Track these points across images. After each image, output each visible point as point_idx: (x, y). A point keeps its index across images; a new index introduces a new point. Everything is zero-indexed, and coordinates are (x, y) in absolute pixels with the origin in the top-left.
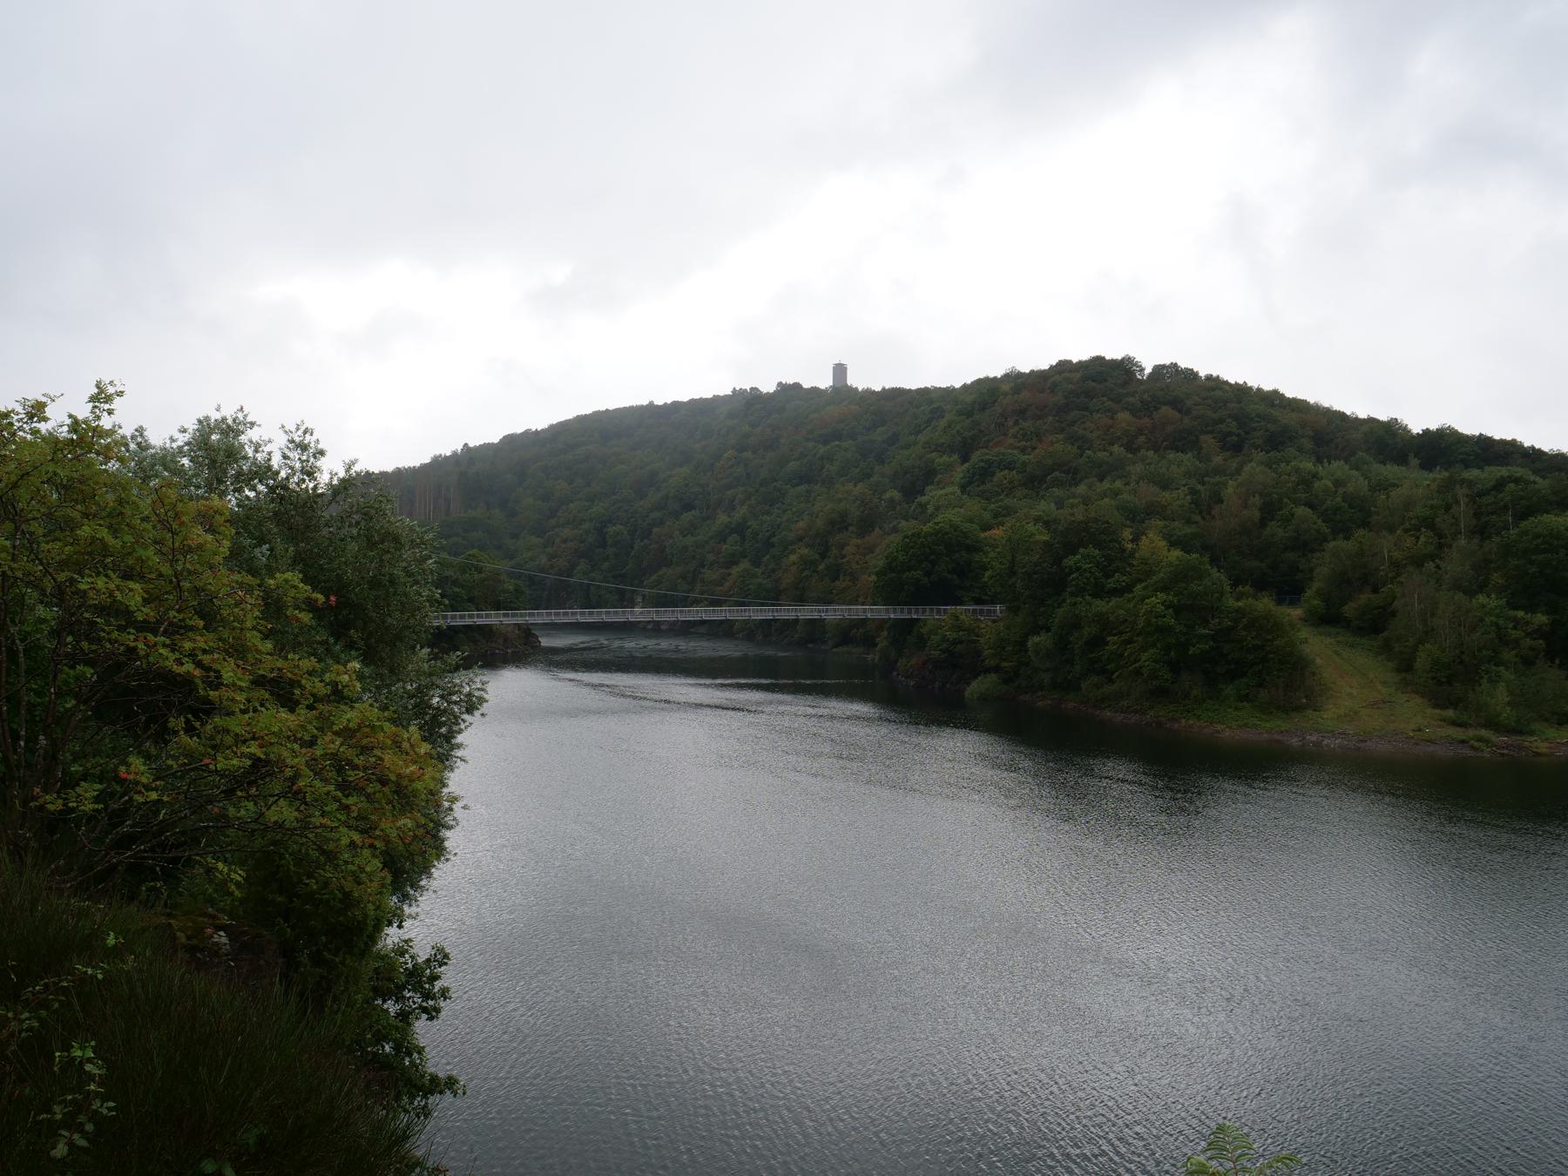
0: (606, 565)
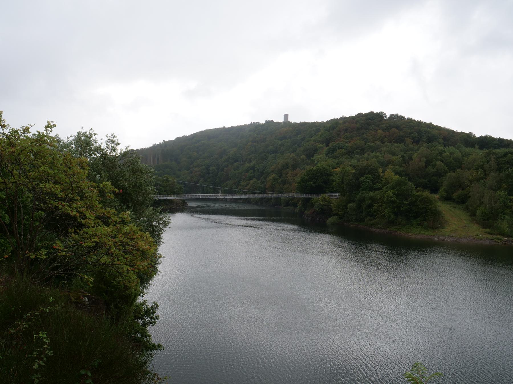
0: (209, 180)
